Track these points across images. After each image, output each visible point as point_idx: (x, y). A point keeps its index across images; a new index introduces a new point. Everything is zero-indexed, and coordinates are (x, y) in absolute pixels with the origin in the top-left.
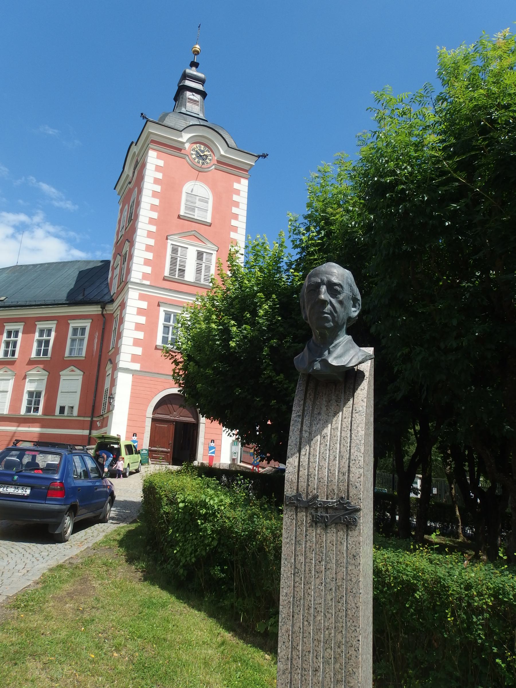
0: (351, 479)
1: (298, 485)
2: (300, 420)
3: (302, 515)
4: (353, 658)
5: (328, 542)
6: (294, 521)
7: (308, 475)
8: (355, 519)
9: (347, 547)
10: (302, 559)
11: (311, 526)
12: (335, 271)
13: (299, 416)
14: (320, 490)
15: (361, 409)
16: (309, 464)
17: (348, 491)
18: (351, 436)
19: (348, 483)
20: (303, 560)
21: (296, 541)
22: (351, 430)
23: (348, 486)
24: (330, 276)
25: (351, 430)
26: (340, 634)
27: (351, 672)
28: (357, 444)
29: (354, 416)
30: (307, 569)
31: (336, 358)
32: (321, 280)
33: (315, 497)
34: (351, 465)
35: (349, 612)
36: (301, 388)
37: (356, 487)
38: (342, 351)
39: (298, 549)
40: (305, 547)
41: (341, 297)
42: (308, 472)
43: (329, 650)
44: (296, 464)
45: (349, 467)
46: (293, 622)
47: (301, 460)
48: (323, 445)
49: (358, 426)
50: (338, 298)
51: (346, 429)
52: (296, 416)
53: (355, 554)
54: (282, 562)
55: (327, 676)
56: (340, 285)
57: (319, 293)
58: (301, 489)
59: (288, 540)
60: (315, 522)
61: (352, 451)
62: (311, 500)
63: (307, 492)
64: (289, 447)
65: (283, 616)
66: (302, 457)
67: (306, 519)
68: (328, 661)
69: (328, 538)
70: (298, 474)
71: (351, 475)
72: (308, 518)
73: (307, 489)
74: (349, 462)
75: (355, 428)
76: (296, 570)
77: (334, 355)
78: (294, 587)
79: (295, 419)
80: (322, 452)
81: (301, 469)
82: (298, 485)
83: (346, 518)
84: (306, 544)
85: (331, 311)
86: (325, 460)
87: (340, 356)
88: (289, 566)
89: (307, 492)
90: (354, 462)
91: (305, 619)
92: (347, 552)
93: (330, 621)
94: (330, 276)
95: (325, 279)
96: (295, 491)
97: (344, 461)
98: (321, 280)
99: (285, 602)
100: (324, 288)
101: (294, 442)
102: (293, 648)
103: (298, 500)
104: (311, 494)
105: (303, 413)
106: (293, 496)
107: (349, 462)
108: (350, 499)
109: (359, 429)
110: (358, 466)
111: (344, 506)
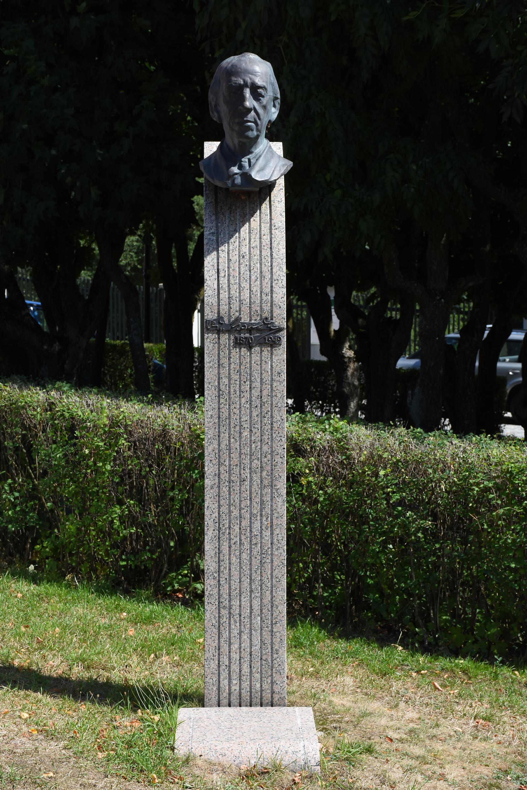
0: (274, 299)
1: (219, 309)
2: (215, 238)
3: (224, 338)
4: (279, 464)
5: (253, 362)
6: (216, 345)
7: (229, 298)
8: (280, 338)
9: (272, 366)
10: (225, 381)
11: (235, 347)
12: (257, 69)
13: (212, 233)
14: (242, 312)
15: (280, 225)
16: (229, 286)
17: (272, 311)
18: (272, 255)
19: (272, 303)
20: (227, 382)
21: (219, 365)
22: (271, 248)
23: (272, 306)
24: (253, 77)
25: (271, 248)
26: (267, 445)
27: (278, 476)
28: (279, 263)
29: (273, 232)
30: (232, 390)
31: (258, 171)
32: (244, 81)
33: (238, 319)
34: (274, 285)
35: (275, 425)
36: (210, 199)
37: (280, 307)
38: (264, 163)
39: (221, 372)
40: (229, 369)
41: (264, 101)
42: (229, 294)
43: (256, 461)
44: (216, 286)
45: (272, 287)
46: (219, 441)
47: (221, 282)
48: (243, 265)
49: (279, 244)
50: (262, 103)
51: (266, 248)
52: (210, 234)
53: (280, 371)
54: (206, 386)
55: (255, 483)
56: (264, 88)
57: (243, 99)
58: (222, 313)
59: (211, 365)
60: (238, 344)
61: (274, 270)
62: (234, 322)
63: (229, 314)
64: (205, 269)
65: (209, 436)
66: (221, 279)
67: (229, 342)
68: (255, 471)
69: (253, 359)
70: (218, 298)
71: (274, 295)
72: (232, 341)
73: (229, 311)
74: (272, 283)
75: (275, 246)
76: (221, 392)
77: (257, 168)
78: (219, 408)
79: (209, 237)
80: (242, 273)
81: (221, 292)
82: (219, 309)
83: (271, 338)
84: (229, 367)
85: (255, 119)
86: (246, 281)
87: (262, 169)
88: (213, 389)
89: (229, 314)
90: (276, 282)
91: (232, 437)
92: (271, 370)
93: (256, 435)
94: (253, 77)
95: (249, 81)
96: (216, 315)
97: (266, 281)
98: (244, 81)
99: (211, 424)
100: (247, 93)
101: (211, 263)
102: (220, 464)
103: (219, 323)
104: (233, 317)
105: (217, 230)
106: (214, 320)
107: (272, 283)
108: (274, 319)
109: (280, 247)
110: (281, 285)
111: (268, 327)
